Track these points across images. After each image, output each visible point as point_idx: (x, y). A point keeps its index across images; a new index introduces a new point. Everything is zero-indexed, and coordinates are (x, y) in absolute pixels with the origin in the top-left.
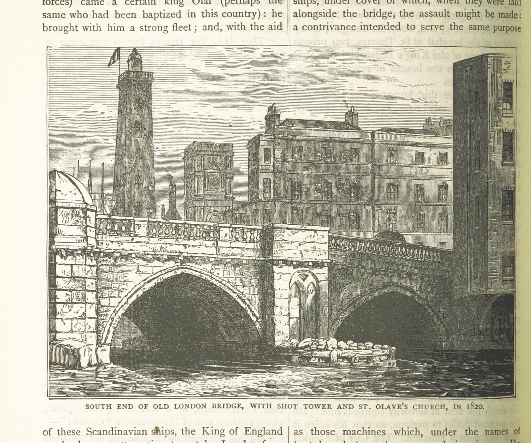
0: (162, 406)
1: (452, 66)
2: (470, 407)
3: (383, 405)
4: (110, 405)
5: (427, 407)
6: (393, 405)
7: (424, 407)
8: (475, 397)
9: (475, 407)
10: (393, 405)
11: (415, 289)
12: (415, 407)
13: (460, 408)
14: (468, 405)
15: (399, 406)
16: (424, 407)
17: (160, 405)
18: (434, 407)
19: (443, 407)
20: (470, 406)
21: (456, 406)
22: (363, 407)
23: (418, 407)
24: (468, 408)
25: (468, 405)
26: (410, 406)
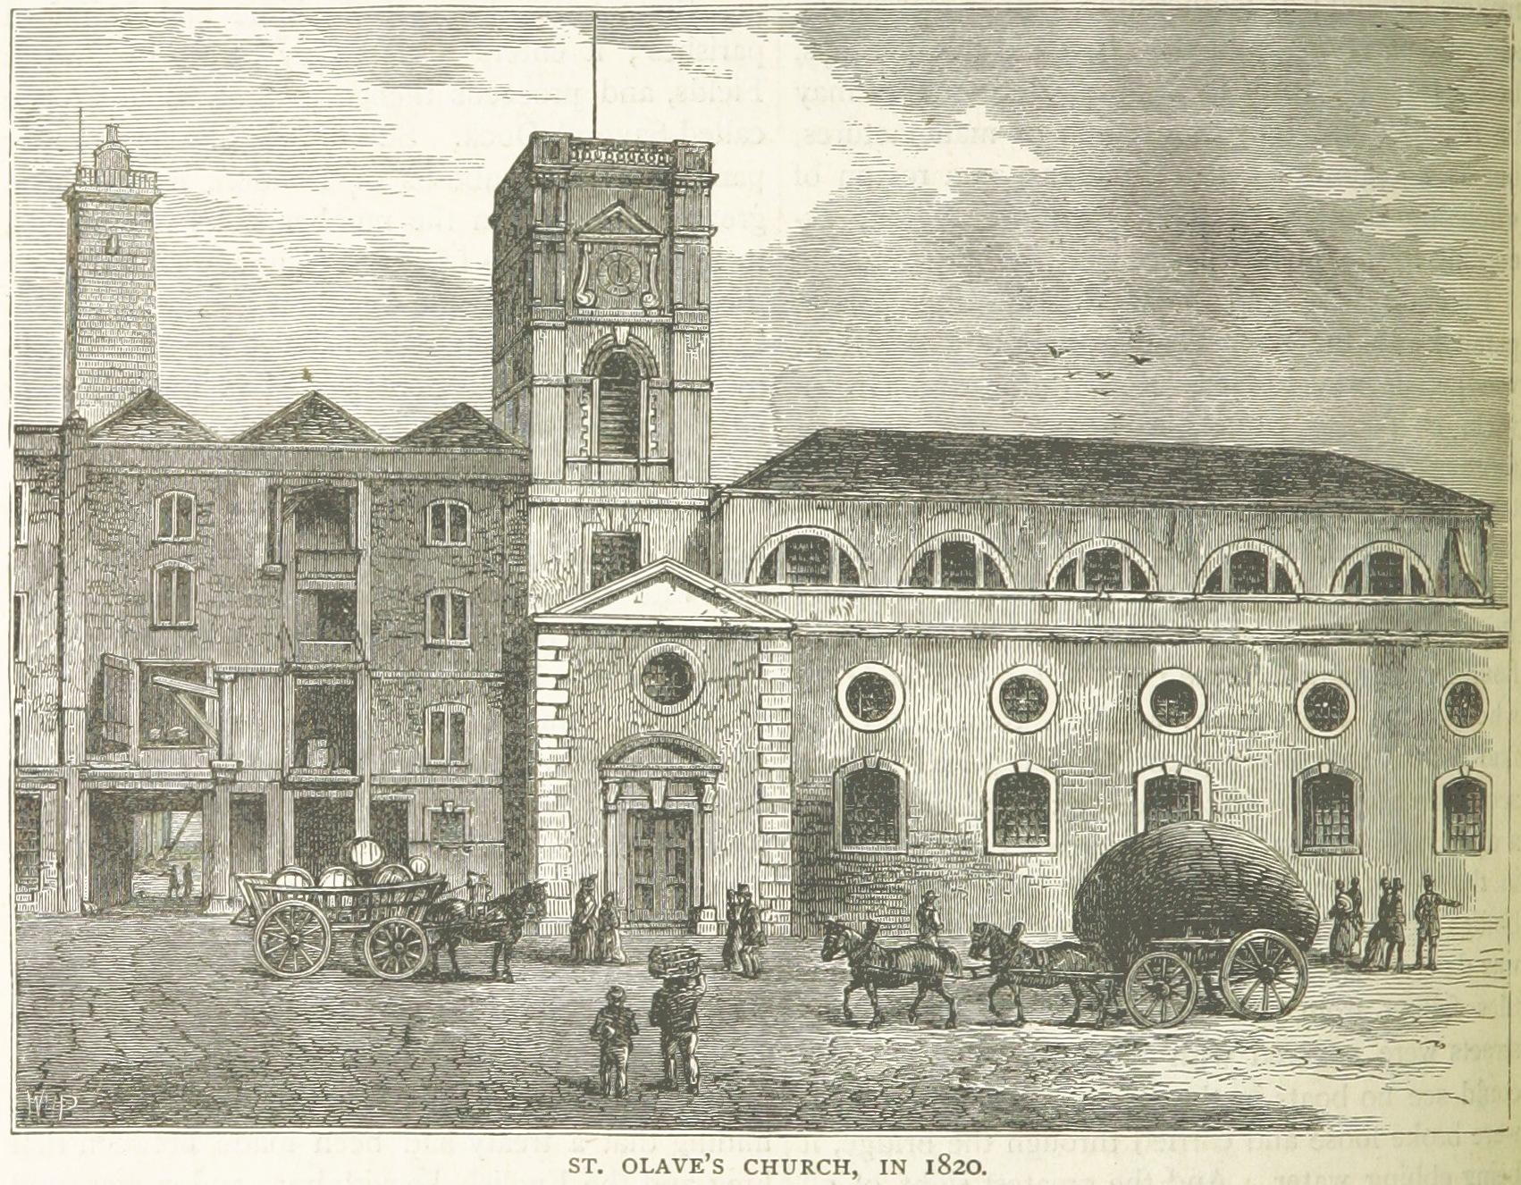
0: (653, 1164)
1: (451, 403)
2: (935, 1169)
3: (644, 1160)
4: (846, 1162)
5: (789, 1165)
6: (676, 1160)
7: (779, 1166)
8: (768, 1128)
9: (954, 1168)
10: (676, 1160)
11: (1027, 989)
12: (751, 1166)
13: (903, 1170)
14: (930, 1162)
15: (695, 1165)
16: (779, 1166)
17: (644, 1160)
18: (814, 1168)
19: (842, 1166)
20: (936, 1165)
21: (889, 1165)
22: (583, 1166)
23: (760, 1167)
24: (930, 1172)
25: (930, 1162)
26: (733, 1163)
